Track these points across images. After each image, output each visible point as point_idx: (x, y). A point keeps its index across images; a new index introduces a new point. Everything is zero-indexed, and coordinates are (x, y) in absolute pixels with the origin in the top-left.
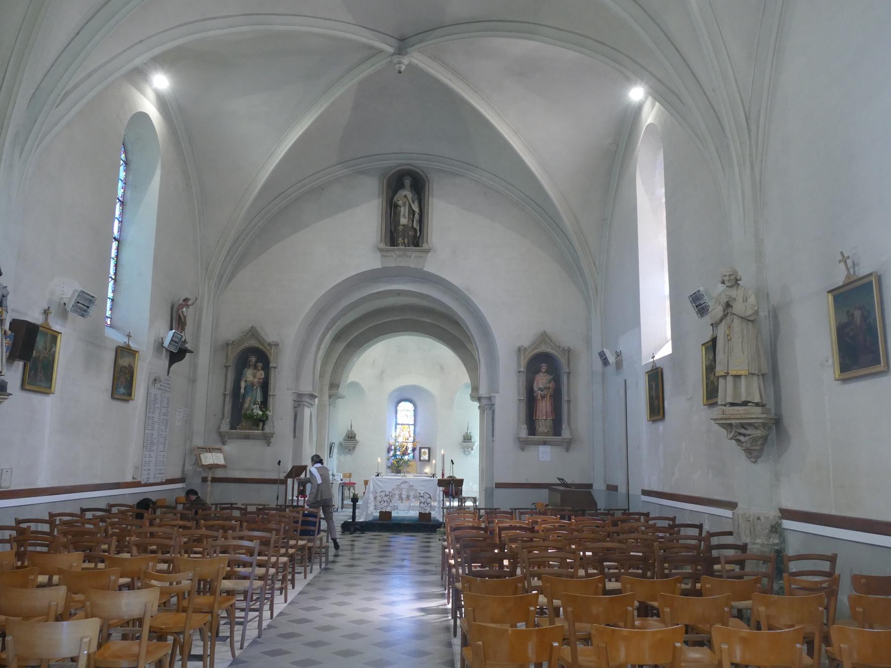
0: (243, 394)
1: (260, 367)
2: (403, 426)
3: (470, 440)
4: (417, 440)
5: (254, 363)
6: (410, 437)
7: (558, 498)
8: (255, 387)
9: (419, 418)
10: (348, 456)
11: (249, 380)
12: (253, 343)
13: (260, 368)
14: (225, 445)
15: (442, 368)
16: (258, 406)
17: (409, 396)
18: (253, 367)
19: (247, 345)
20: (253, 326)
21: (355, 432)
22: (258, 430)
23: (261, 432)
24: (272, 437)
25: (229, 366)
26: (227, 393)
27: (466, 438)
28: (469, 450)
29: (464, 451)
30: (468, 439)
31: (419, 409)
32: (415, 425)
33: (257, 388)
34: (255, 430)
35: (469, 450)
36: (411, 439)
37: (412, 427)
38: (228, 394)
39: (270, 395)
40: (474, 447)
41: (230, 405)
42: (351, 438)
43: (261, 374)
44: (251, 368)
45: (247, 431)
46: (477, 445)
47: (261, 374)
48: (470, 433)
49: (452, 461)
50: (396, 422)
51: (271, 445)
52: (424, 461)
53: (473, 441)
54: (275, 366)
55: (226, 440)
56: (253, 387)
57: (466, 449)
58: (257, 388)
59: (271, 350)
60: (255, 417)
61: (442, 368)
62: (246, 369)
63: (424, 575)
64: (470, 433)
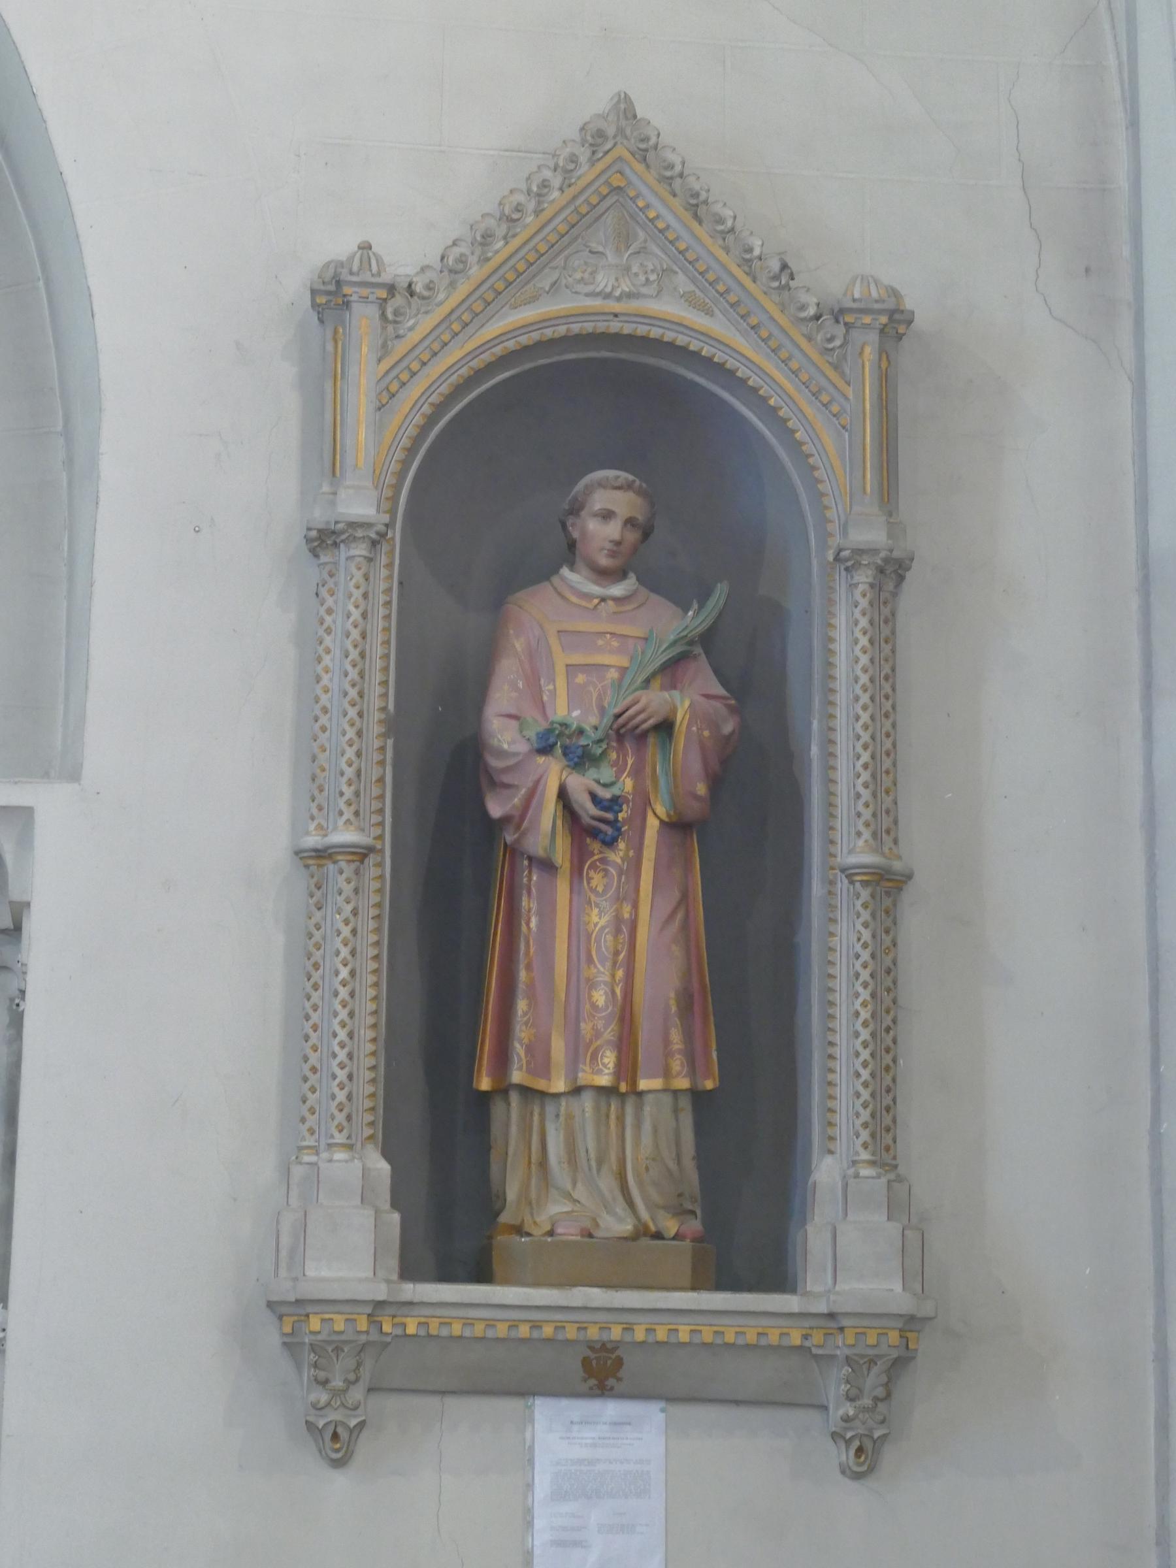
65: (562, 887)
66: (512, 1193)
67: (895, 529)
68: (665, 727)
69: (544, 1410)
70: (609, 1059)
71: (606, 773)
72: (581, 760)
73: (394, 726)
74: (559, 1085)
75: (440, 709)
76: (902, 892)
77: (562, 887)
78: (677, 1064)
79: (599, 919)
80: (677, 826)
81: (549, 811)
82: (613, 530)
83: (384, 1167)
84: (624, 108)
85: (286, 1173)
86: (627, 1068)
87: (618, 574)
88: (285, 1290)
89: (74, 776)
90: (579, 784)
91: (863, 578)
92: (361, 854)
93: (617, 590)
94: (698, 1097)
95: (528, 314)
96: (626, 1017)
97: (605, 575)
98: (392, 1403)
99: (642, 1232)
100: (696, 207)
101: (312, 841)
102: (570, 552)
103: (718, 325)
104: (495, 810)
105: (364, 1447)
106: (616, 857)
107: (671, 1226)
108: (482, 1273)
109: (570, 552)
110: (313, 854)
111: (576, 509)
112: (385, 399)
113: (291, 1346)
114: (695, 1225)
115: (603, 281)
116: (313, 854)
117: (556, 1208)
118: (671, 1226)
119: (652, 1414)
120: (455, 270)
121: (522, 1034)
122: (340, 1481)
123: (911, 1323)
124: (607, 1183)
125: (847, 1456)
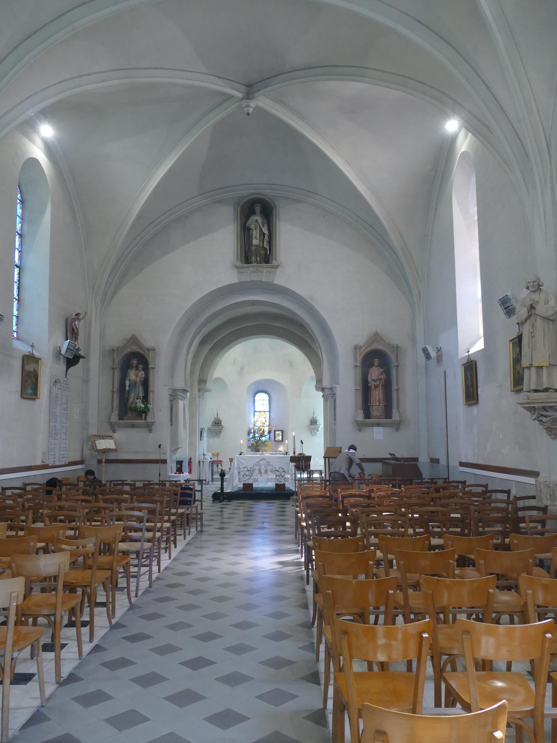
0: (128, 391)
2: (260, 413)
3: (316, 423)
4: (272, 424)
6: (266, 421)
8: (137, 385)
9: (272, 406)
10: (216, 439)
12: (134, 348)
15: (291, 365)
17: (265, 388)
18: (135, 369)
19: (130, 350)
21: (220, 419)
22: (141, 420)
23: (144, 421)
24: (153, 425)
25: (116, 368)
27: (312, 422)
28: (316, 431)
29: (311, 433)
30: (314, 423)
31: (273, 399)
32: (270, 412)
35: (316, 431)
36: (267, 424)
37: (268, 414)
40: (319, 429)
42: (218, 424)
44: (133, 369)
48: (316, 417)
49: (301, 441)
50: (254, 410)
52: (279, 441)
53: (318, 423)
56: (136, 384)
57: (312, 431)
58: (139, 385)
59: (149, 354)
61: (291, 365)
62: (129, 370)
64: (316, 417)
65: (374, 390)
66: (371, 412)
67: (397, 363)
68: (381, 379)
69: (374, 428)
70: (378, 403)
71: (377, 382)
72: (375, 381)
73: (361, 379)
74: (374, 405)
75: (467, 521)
76: (222, 424)
77: (374, 390)
78: (383, 403)
79: (377, 393)
80: (382, 386)
81: (373, 385)
82: (377, 364)
83: (362, 411)
84: (377, 332)
85: (356, 412)
86: (379, 403)
87: (377, 367)
88: (356, 420)
89: (339, 384)
90: (375, 383)
91: (395, 367)
92: (359, 389)
93: (377, 368)
94: (385, 405)
95: (370, 348)
96: (379, 399)
97: (376, 367)
98: (364, 427)
99: (381, 415)
100: (382, 339)
101: (356, 388)
102: (374, 365)
103: (384, 348)
104: (369, 385)
105: (362, 431)
106: (378, 388)
107: (383, 414)
108: (370, 418)
109: (374, 365)
110: (207, 349)
111: (374, 362)
112: (360, 355)
113: (357, 424)
114: (385, 414)
115: (375, 346)
116: (207, 348)
117: (374, 413)
118: (383, 414)
119: (382, 428)
120: (364, 345)
121: (372, 401)
122: (360, 433)
123: (400, 421)
124: (378, 412)
125: (395, 430)
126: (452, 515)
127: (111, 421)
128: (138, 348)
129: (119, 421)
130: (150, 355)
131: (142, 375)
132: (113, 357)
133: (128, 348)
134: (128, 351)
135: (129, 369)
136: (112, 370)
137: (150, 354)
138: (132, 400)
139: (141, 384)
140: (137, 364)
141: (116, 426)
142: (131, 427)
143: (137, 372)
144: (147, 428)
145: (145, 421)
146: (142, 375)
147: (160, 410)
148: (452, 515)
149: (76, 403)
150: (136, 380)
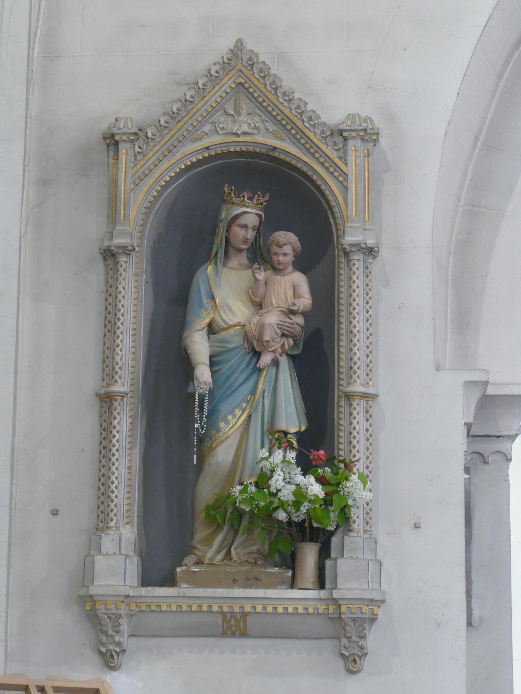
0: (211, 391)
1: (288, 249)
5: (251, 234)
7: (256, 265)
8: (266, 359)
11: (232, 320)
12: (245, 128)
13: (290, 258)
14: (113, 669)
16: (292, 455)
18: (243, 258)
19: (216, 139)
20: (239, 44)
22: (293, 584)
23: (312, 594)
24: (373, 619)
25: (126, 250)
26: (117, 388)
33: (276, 363)
34: (274, 586)
38: (123, 395)
39: (349, 396)
41: (137, 452)
43: (295, 288)
44: (234, 262)
45: (237, 592)
46: (210, 270)
47: (295, 288)
51: (367, 664)
54: (371, 242)
55: (123, 638)
56: (257, 355)
58: (276, 363)
59: (344, 158)
60: (281, 516)
62: (210, 268)
63: (331, 208)
126: (195, 463)
127: (93, 591)
128: (271, 127)
129: (144, 591)
130: (351, 170)
131: (296, 295)
132: (114, 183)
133: (207, 128)
134: (206, 142)
135: (206, 259)
136: (100, 266)
137: (351, 158)
138: (230, 457)
139: (293, 358)
140: (258, 230)
141: (125, 626)
142: (224, 635)
143: (261, 276)
144: (327, 643)
145: (323, 594)
146: (296, 295)
147: (417, 526)
148: (195, 463)
149: (192, 140)
150: (261, 328)
